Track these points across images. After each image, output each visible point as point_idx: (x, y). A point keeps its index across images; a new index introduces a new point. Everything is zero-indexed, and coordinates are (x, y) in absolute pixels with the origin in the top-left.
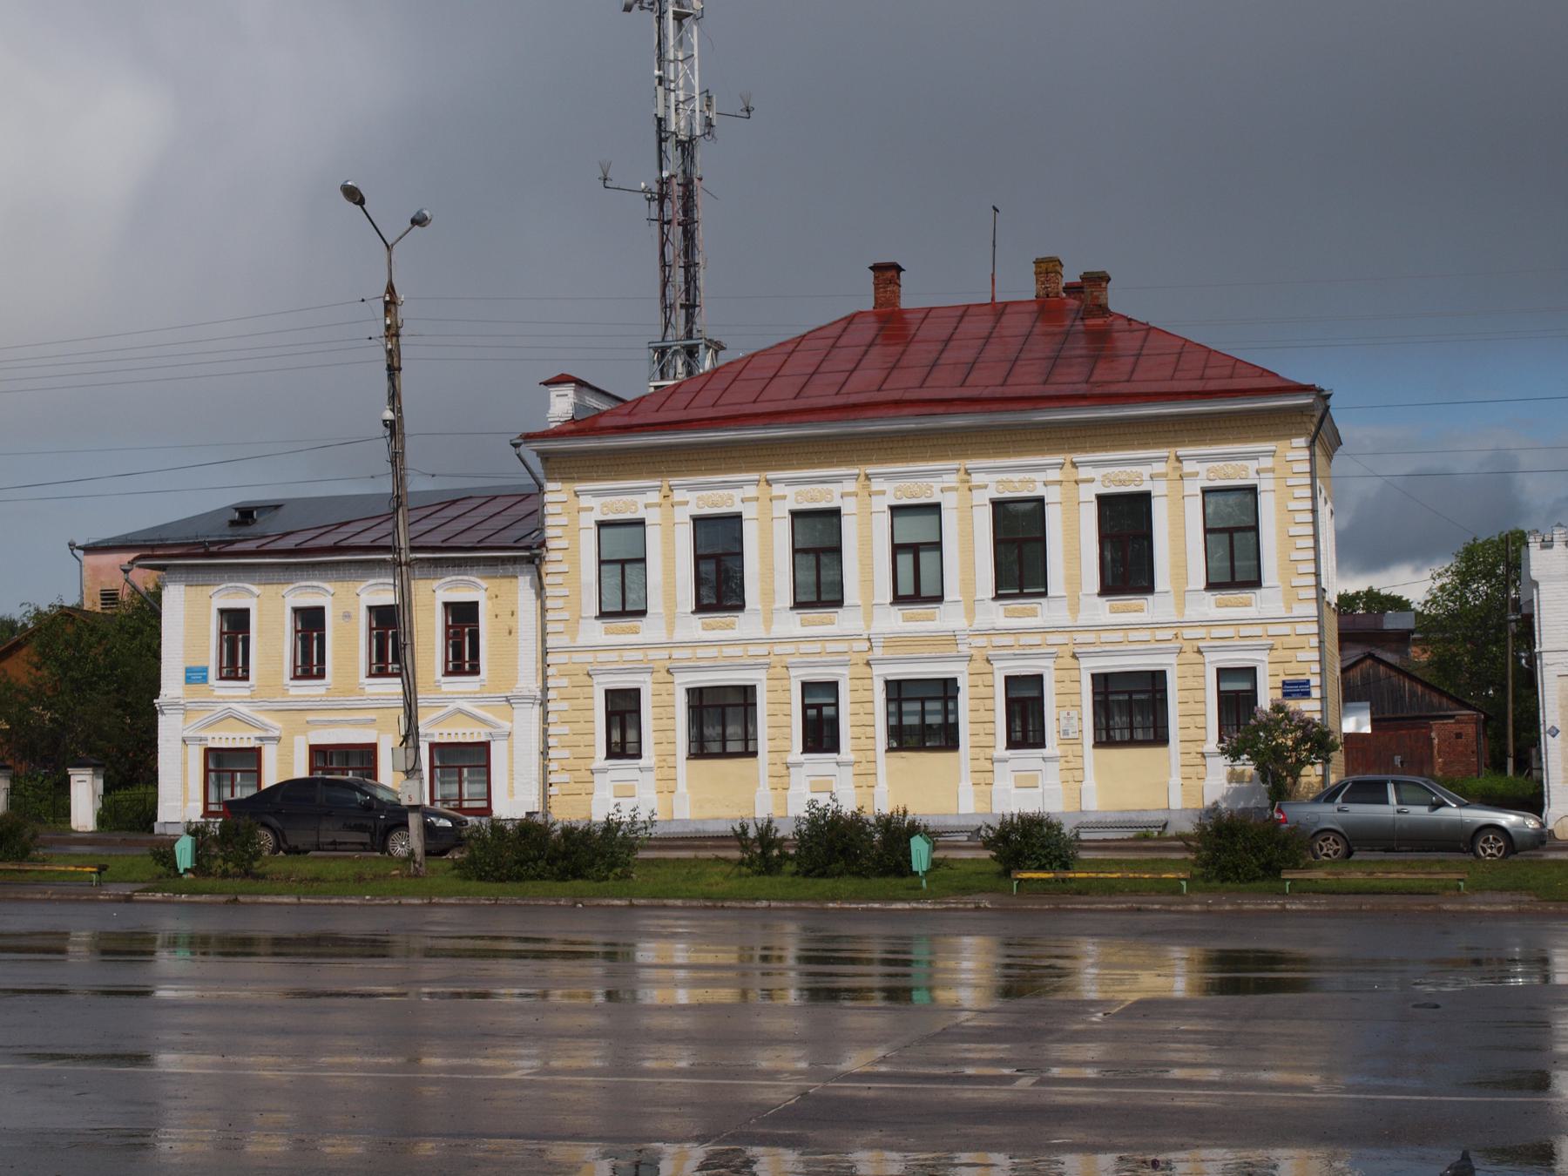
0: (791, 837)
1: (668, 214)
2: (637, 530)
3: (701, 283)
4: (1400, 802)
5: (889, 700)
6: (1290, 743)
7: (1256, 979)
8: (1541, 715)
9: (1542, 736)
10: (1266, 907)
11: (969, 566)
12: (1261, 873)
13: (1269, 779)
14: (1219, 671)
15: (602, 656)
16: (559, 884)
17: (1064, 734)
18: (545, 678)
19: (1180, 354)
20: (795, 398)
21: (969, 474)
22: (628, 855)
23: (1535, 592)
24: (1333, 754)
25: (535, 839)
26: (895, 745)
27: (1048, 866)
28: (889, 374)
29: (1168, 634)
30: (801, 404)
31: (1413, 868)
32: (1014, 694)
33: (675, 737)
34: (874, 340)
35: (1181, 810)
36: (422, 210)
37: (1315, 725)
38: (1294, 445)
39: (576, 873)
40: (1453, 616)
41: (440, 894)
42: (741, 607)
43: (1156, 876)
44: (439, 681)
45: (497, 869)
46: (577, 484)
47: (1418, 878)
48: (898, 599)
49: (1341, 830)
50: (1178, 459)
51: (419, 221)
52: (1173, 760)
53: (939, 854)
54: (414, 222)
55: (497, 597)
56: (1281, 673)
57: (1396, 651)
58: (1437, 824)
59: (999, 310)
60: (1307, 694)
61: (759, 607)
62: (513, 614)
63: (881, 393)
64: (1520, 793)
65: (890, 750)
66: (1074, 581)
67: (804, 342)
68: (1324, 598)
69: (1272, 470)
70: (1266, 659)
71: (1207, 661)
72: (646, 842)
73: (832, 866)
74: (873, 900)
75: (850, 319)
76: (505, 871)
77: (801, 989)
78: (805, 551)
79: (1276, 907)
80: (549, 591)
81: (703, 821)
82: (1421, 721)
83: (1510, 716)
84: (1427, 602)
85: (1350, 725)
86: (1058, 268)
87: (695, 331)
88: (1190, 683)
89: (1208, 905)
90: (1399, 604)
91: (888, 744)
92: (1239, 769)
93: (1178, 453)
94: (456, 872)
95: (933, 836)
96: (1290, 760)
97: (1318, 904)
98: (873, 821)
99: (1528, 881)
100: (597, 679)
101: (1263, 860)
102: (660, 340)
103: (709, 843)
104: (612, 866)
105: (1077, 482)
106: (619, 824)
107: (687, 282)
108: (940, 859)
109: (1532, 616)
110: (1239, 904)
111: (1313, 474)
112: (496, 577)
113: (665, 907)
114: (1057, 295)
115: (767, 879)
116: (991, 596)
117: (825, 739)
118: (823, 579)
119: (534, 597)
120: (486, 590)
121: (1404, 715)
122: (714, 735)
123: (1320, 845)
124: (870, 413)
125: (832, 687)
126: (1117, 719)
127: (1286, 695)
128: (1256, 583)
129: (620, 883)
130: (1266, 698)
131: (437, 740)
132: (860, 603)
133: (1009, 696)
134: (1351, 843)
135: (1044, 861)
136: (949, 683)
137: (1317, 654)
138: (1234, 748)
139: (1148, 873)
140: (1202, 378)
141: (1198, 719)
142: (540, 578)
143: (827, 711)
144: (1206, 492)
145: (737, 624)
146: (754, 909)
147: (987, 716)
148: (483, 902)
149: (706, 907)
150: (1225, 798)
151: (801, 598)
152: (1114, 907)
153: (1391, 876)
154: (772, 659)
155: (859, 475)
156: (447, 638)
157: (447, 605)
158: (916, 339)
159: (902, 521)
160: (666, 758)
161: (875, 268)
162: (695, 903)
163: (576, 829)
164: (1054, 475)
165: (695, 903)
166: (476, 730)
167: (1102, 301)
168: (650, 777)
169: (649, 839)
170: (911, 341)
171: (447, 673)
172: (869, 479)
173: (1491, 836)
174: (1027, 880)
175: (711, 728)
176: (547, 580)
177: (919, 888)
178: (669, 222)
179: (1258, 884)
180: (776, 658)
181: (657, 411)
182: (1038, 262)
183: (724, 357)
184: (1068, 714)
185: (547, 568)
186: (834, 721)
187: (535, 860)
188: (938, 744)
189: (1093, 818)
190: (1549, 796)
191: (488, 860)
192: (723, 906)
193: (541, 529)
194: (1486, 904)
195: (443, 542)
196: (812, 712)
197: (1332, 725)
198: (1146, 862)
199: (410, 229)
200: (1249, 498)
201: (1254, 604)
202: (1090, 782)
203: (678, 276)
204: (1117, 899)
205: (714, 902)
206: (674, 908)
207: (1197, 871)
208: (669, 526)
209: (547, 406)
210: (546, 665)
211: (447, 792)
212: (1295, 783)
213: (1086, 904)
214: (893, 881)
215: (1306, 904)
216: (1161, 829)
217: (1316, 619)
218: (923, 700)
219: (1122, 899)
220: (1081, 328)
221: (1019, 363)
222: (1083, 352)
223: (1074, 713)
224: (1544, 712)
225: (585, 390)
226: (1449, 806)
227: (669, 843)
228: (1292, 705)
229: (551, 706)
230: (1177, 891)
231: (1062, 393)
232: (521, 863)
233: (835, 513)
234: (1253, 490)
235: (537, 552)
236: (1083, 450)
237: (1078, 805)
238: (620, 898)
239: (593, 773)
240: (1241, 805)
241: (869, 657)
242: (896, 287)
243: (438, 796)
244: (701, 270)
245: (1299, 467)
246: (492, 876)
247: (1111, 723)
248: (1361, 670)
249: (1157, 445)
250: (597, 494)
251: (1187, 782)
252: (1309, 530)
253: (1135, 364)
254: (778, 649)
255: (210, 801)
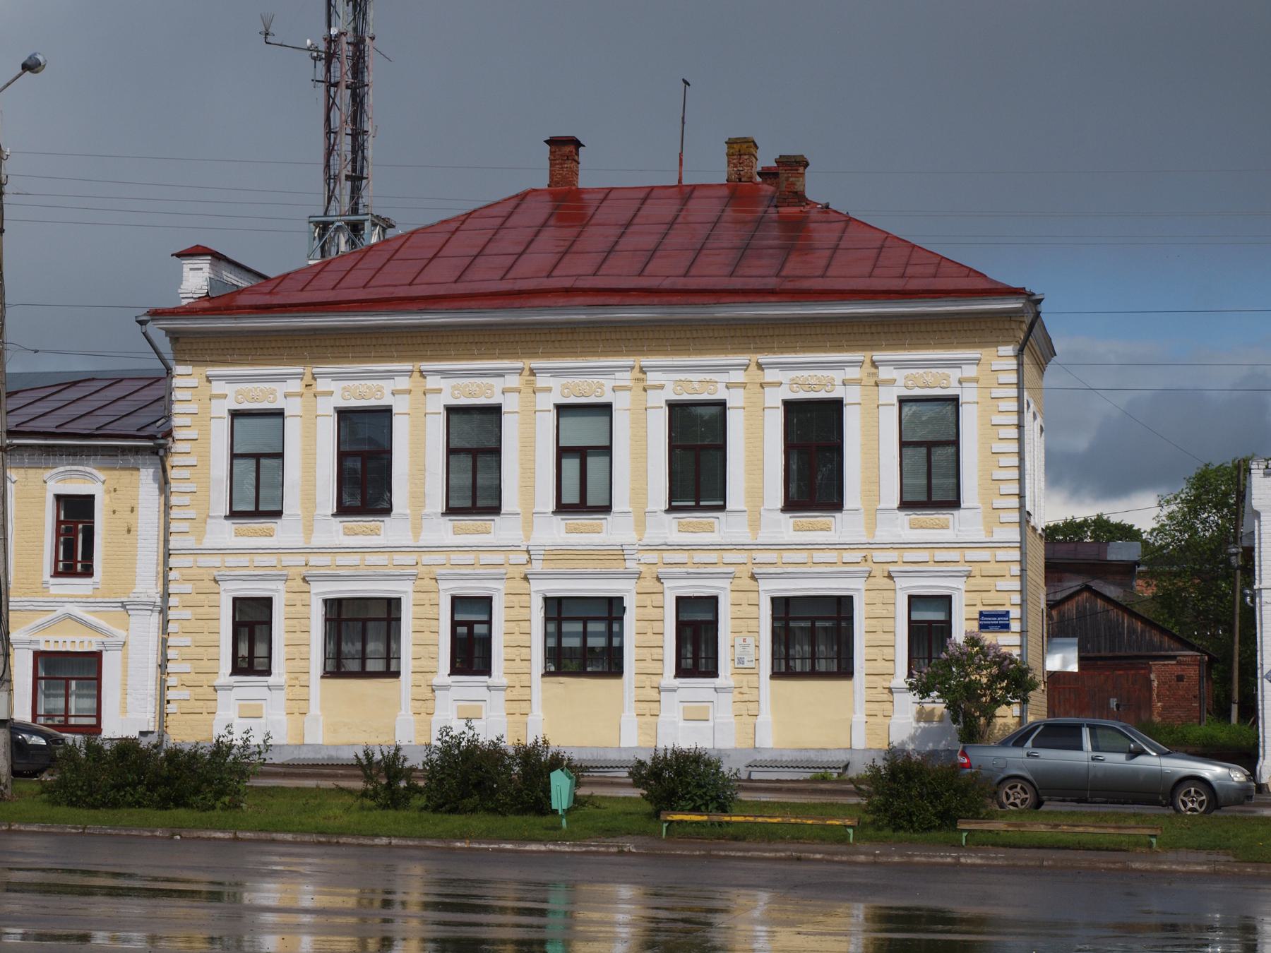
0: (421, 767)
1: (336, 75)
2: (275, 421)
3: (369, 153)
4: (1095, 748)
5: (547, 619)
6: (984, 680)
7: (929, 941)
8: (1259, 658)
9: (1259, 681)
10: (938, 860)
11: (640, 474)
12: (938, 822)
13: (961, 719)
14: (911, 598)
15: (231, 561)
16: (159, 812)
17: (739, 663)
18: (166, 582)
19: (881, 248)
20: (455, 282)
21: (645, 373)
22: (238, 782)
23: (1256, 523)
24: (1031, 693)
25: (135, 762)
26: (553, 669)
27: (703, 808)
28: (561, 259)
29: (856, 556)
30: (461, 288)
31: (1106, 821)
32: (686, 617)
33: (309, 653)
34: (547, 220)
35: (865, 750)
36: (35, 54)
37: (1012, 661)
38: (1000, 353)
39: (179, 801)
40: (1189, 545)
41: (21, 822)
42: (387, 511)
43: (820, 822)
44: (47, 583)
45: (91, 794)
46: (209, 369)
47: (1107, 832)
48: (562, 508)
49: (1030, 777)
50: (874, 364)
51: (31, 66)
52: (857, 697)
53: (584, 792)
54: (26, 67)
55: (115, 490)
56: (979, 602)
57: (1120, 585)
58: (1135, 775)
59: (685, 193)
60: (1005, 627)
61: (408, 511)
62: (132, 511)
63: (550, 279)
64: (1244, 743)
65: (547, 674)
66: (756, 495)
67: (469, 220)
68: (1028, 522)
69: (976, 380)
70: (963, 587)
71: (898, 587)
72: (259, 769)
73: (465, 801)
74: (506, 840)
75: (522, 197)
76: (99, 797)
77: (424, 940)
78: (684, 448)
79: (949, 860)
80: (174, 486)
81: (336, 747)
82: (1140, 661)
83: (1236, 659)
84: (1153, 530)
85: (1054, 663)
86: (752, 150)
87: (360, 206)
88: (879, 610)
89: (875, 855)
90: (1127, 533)
91: (545, 668)
92: (928, 707)
93: (874, 358)
94: (45, 796)
95: (578, 771)
96: (984, 699)
97: (996, 858)
98: (511, 752)
99: (1228, 840)
100: (223, 585)
101: (940, 808)
102: (322, 215)
103: (340, 772)
104: (219, 794)
105: (762, 385)
106: (230, 747)
107: (354, 151)
108: (584, 796)
109: (1253, 549)
110: (909, 856)
111: (1020, 386)
112: (115, 469)
113: (273, 841)
114: (751, 179)
115: (391, 812)
116: (664, 509)
117: (476, 660)
118: (480, 482)
119: (157, 492)
120: (104, 482)
121: (1122, 654)
122: (353, 652)
123: (1007, 793)
124: (536, 302)
125: (485, 603)
126: (822, 648)
127: (983, 627)
128: (955, 504)
129: (227, 813)
130: (961, 628)
131: (43, 647)
132: (519, 510)
133: (681, 618)
134: (1040, 792)
135: (699, 802)
136: (614, 602)
137: (1018, 583)
138: (923, 684)
139: (812, 818)
140: (902, 276)
141: (886, 650)
142: (164, 471)
143: (479, 630)
144: (903, 401)
145: (382, 529)
146: (372, 846)
147: (523, 640)
148: (69, 830)
149: (320, 843)
150: (913, 738)
151: (454, 503)
152: (772, 855)
153: (1077, 829)
154: (420, 569)
155: (523, 369)
156: (58, 534)
157: (59, 498)
158: (593, 222)
159: (568, 422)
160: (298, 677)
161: (552, 142)
162: (307, 838)
163: (181, 751)
164: (737, 376)
165: (307, 838)
166: (86, 638)
167: (798, 188)
168: (280, 696)
169: (263, 764)
170: (587, 223)
171: (57, 574)
172: (534, 375)
173: (1193, 789)
174: (680, 822)
175: (350, 644)
176: (172, 474)
177: (558, 828)
178: (336, 85)
179: (934, 834)
180: (424, 569)
181: (302, 290)
182: (730, 143)
183: (390, 233)
184: (744, 640)
185: (173, 460)
186: (487, 641)
187: (134, 785)
188: (600, 669)
189: (767, 757)
190: (1264, 746)
191: (80, 784)
192: (338, 842)
193: (168, 417)
194: (1179, 863)
195: (57, 427)
196: (462, 630)
197: (1032, 661)
198: (814, 806)
199: (20, 75)
200: (949, 408)
201: (951, 527)
202: (766, 716)
203: (345, 144)
204: (775, 847)
205: (328, 837)
206: (284, 842)
207: (868, 818)
208: (311, 419)
209: (180, 281)
210: (168, 569)
211: (52, 707)
212: (989, 724)
213: (740, 850)
214: (531, 819)
215: (982, 858)
216: (841, 771)
217: (1018, 545)
218: (585, 621)
219: (781, 846)
220: (774, 216)
221: (704, 252)
222: (776, 242)
223: (750, 640)
224: (1262, 656)
225: (223, 264)
226: (1150, 754)
227: (296, 771)
228: (989, 638)
229: (172, 614)
230: (843, 840)
231: (750, 287)
232: (117, 787)
233: (495, 411)
234: (954, 400)
235: (162, 441)
236: (771, 350)
237: (751, 742)
238: (223, 830)
239: (216, 690)
240: (930, 746)
241: (528, 571)
242: (574, 163)
243: (41, 711)
244: (370, 139)
245: (1004, 378)
246: (84, 802)
247: (792, 652)
248: (1077, 603)
249: (851, 348)
250: (231, 379)
251: (872, 719)
252: (1014, 447)
253: (832, 258)
254: (427, 559)
255: (38, 713)
